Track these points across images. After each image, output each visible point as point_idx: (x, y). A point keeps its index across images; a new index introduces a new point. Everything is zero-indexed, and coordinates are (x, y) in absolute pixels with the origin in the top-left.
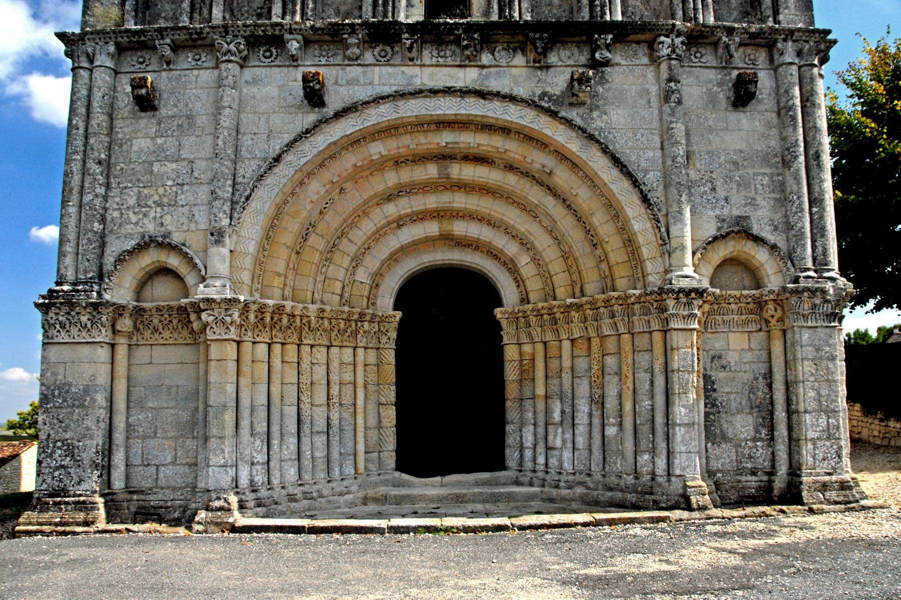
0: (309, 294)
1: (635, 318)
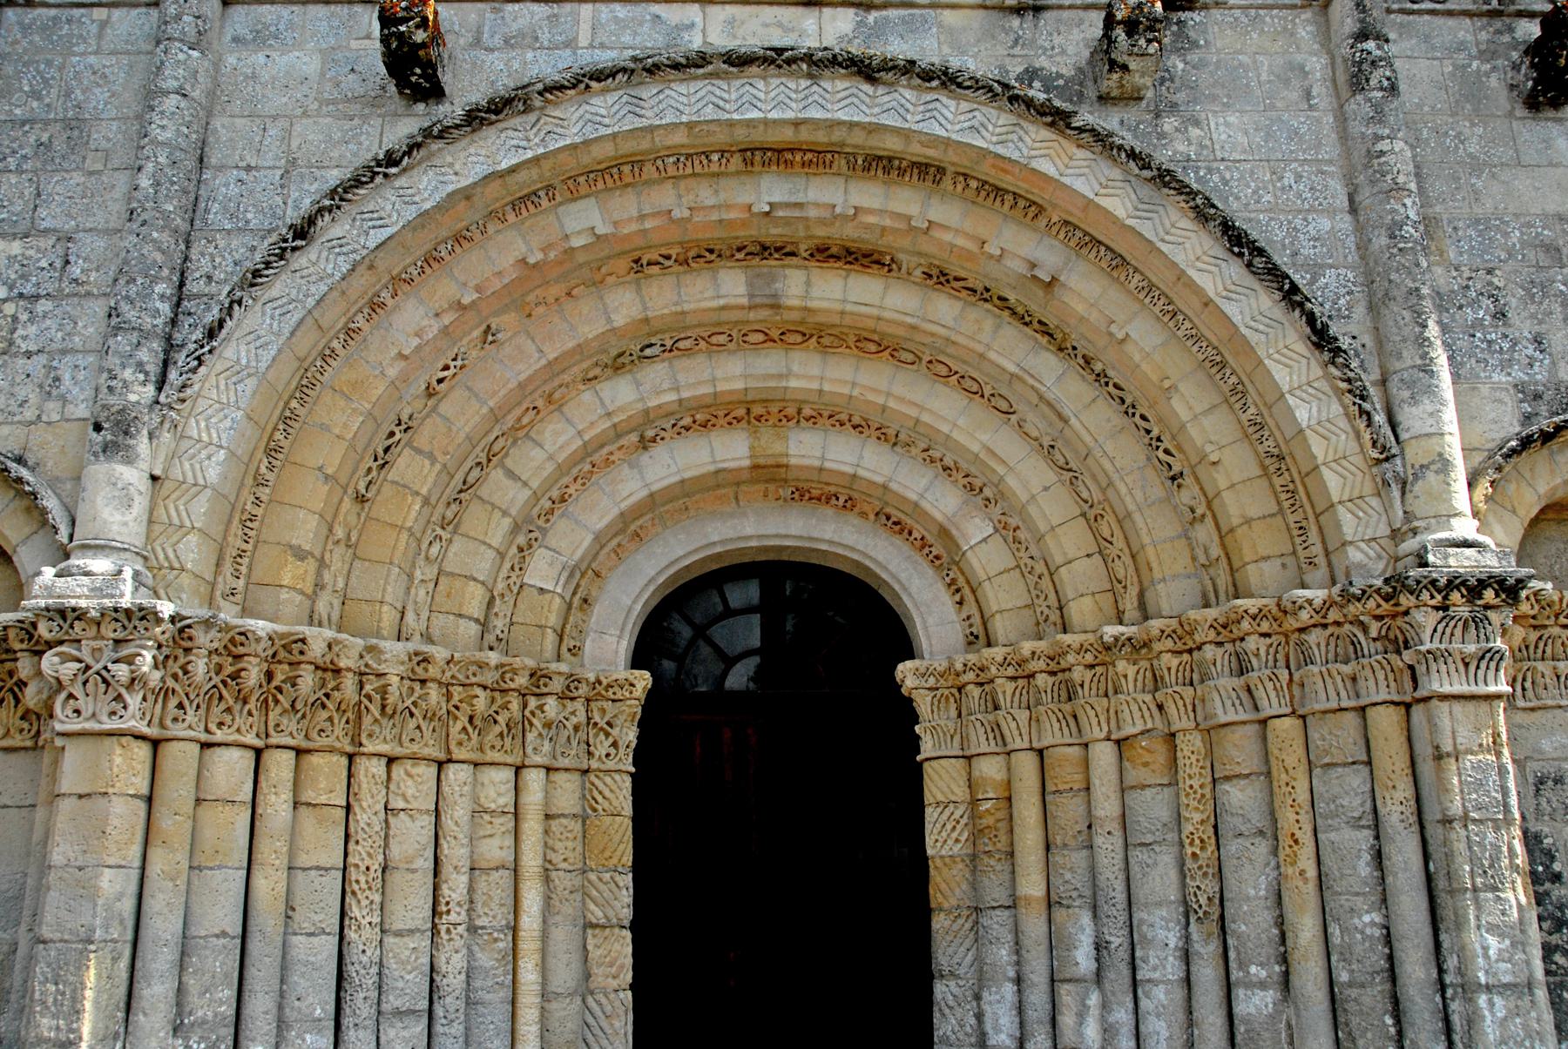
0: (388, 617)
1: (1315, 669)
